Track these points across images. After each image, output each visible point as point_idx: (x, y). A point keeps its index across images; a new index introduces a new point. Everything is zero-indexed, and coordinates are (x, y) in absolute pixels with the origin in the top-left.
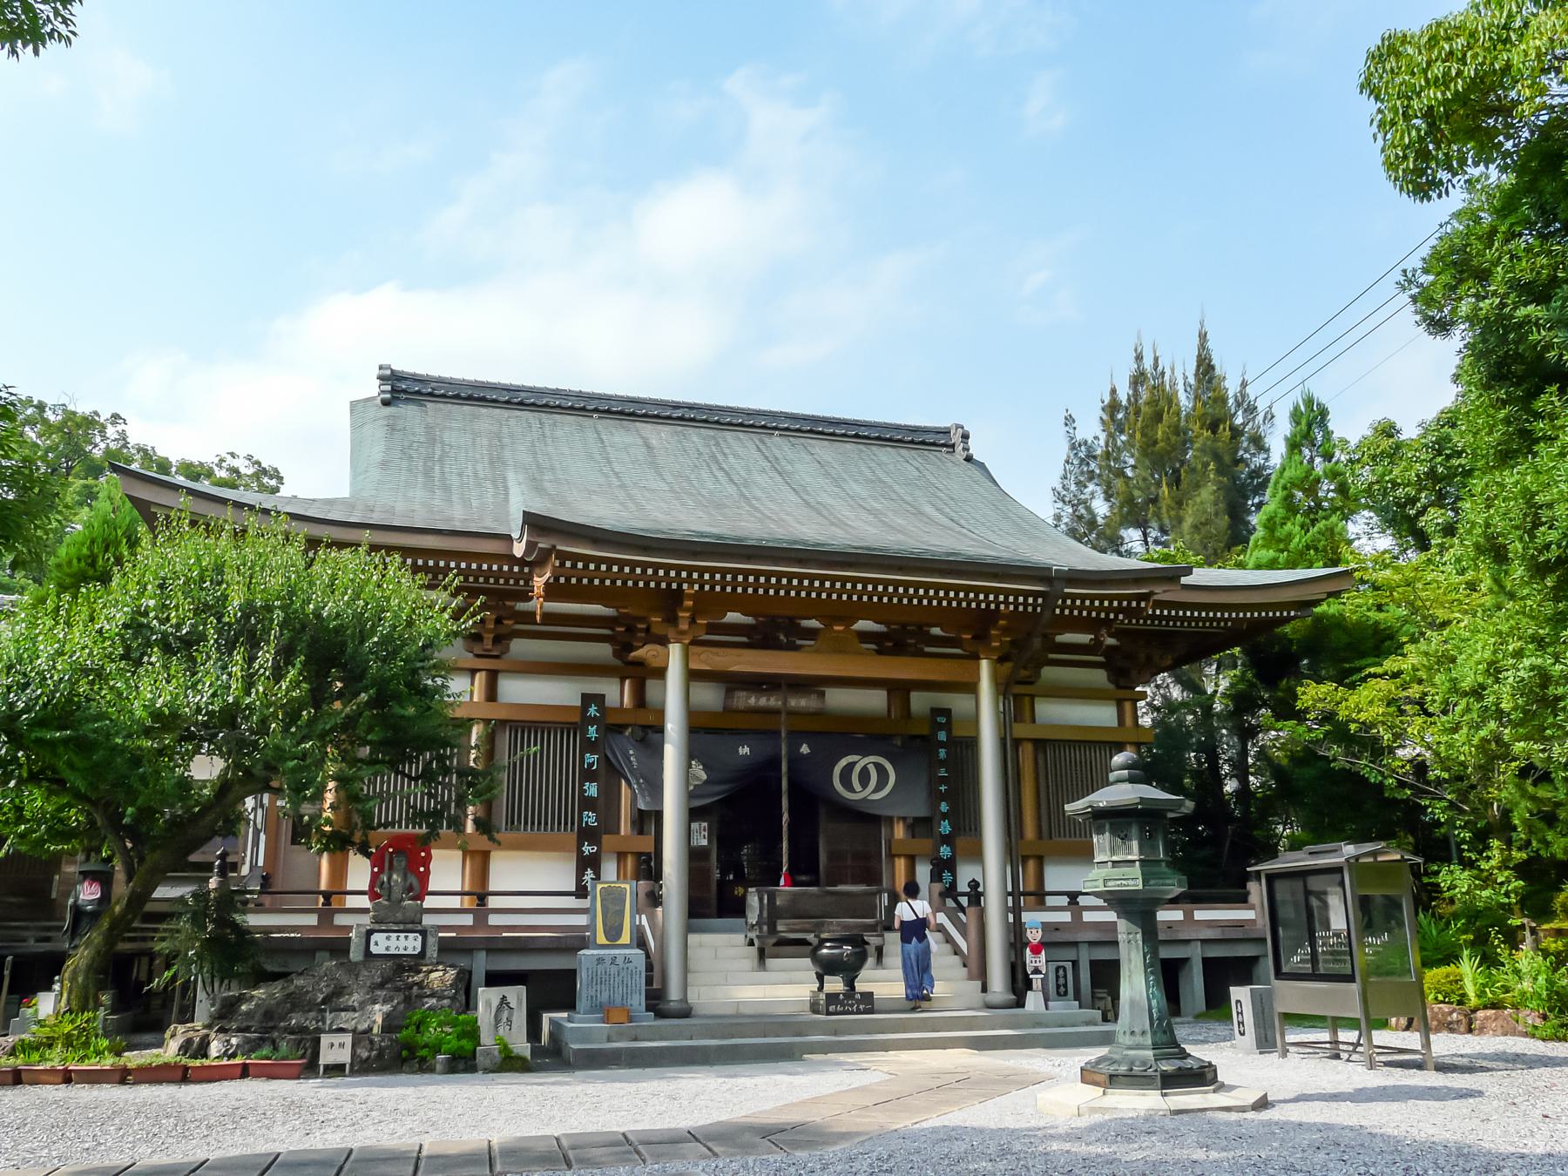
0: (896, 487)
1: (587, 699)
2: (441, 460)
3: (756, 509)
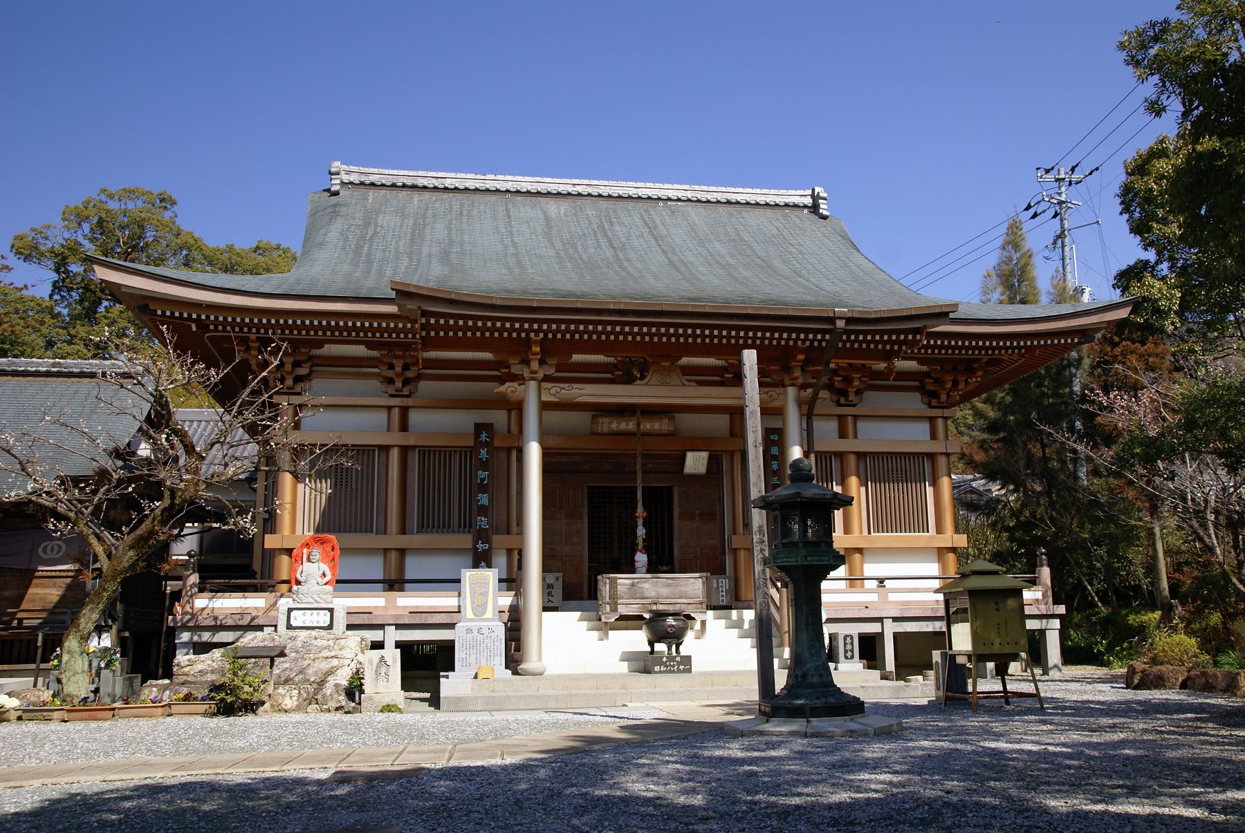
0: (755, 246)
1: (479, 428)
2: (371, 239)
3: (624, 269)
